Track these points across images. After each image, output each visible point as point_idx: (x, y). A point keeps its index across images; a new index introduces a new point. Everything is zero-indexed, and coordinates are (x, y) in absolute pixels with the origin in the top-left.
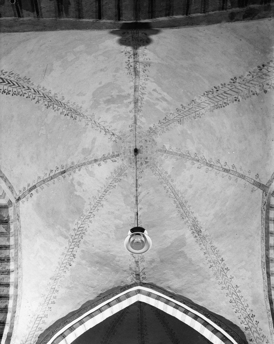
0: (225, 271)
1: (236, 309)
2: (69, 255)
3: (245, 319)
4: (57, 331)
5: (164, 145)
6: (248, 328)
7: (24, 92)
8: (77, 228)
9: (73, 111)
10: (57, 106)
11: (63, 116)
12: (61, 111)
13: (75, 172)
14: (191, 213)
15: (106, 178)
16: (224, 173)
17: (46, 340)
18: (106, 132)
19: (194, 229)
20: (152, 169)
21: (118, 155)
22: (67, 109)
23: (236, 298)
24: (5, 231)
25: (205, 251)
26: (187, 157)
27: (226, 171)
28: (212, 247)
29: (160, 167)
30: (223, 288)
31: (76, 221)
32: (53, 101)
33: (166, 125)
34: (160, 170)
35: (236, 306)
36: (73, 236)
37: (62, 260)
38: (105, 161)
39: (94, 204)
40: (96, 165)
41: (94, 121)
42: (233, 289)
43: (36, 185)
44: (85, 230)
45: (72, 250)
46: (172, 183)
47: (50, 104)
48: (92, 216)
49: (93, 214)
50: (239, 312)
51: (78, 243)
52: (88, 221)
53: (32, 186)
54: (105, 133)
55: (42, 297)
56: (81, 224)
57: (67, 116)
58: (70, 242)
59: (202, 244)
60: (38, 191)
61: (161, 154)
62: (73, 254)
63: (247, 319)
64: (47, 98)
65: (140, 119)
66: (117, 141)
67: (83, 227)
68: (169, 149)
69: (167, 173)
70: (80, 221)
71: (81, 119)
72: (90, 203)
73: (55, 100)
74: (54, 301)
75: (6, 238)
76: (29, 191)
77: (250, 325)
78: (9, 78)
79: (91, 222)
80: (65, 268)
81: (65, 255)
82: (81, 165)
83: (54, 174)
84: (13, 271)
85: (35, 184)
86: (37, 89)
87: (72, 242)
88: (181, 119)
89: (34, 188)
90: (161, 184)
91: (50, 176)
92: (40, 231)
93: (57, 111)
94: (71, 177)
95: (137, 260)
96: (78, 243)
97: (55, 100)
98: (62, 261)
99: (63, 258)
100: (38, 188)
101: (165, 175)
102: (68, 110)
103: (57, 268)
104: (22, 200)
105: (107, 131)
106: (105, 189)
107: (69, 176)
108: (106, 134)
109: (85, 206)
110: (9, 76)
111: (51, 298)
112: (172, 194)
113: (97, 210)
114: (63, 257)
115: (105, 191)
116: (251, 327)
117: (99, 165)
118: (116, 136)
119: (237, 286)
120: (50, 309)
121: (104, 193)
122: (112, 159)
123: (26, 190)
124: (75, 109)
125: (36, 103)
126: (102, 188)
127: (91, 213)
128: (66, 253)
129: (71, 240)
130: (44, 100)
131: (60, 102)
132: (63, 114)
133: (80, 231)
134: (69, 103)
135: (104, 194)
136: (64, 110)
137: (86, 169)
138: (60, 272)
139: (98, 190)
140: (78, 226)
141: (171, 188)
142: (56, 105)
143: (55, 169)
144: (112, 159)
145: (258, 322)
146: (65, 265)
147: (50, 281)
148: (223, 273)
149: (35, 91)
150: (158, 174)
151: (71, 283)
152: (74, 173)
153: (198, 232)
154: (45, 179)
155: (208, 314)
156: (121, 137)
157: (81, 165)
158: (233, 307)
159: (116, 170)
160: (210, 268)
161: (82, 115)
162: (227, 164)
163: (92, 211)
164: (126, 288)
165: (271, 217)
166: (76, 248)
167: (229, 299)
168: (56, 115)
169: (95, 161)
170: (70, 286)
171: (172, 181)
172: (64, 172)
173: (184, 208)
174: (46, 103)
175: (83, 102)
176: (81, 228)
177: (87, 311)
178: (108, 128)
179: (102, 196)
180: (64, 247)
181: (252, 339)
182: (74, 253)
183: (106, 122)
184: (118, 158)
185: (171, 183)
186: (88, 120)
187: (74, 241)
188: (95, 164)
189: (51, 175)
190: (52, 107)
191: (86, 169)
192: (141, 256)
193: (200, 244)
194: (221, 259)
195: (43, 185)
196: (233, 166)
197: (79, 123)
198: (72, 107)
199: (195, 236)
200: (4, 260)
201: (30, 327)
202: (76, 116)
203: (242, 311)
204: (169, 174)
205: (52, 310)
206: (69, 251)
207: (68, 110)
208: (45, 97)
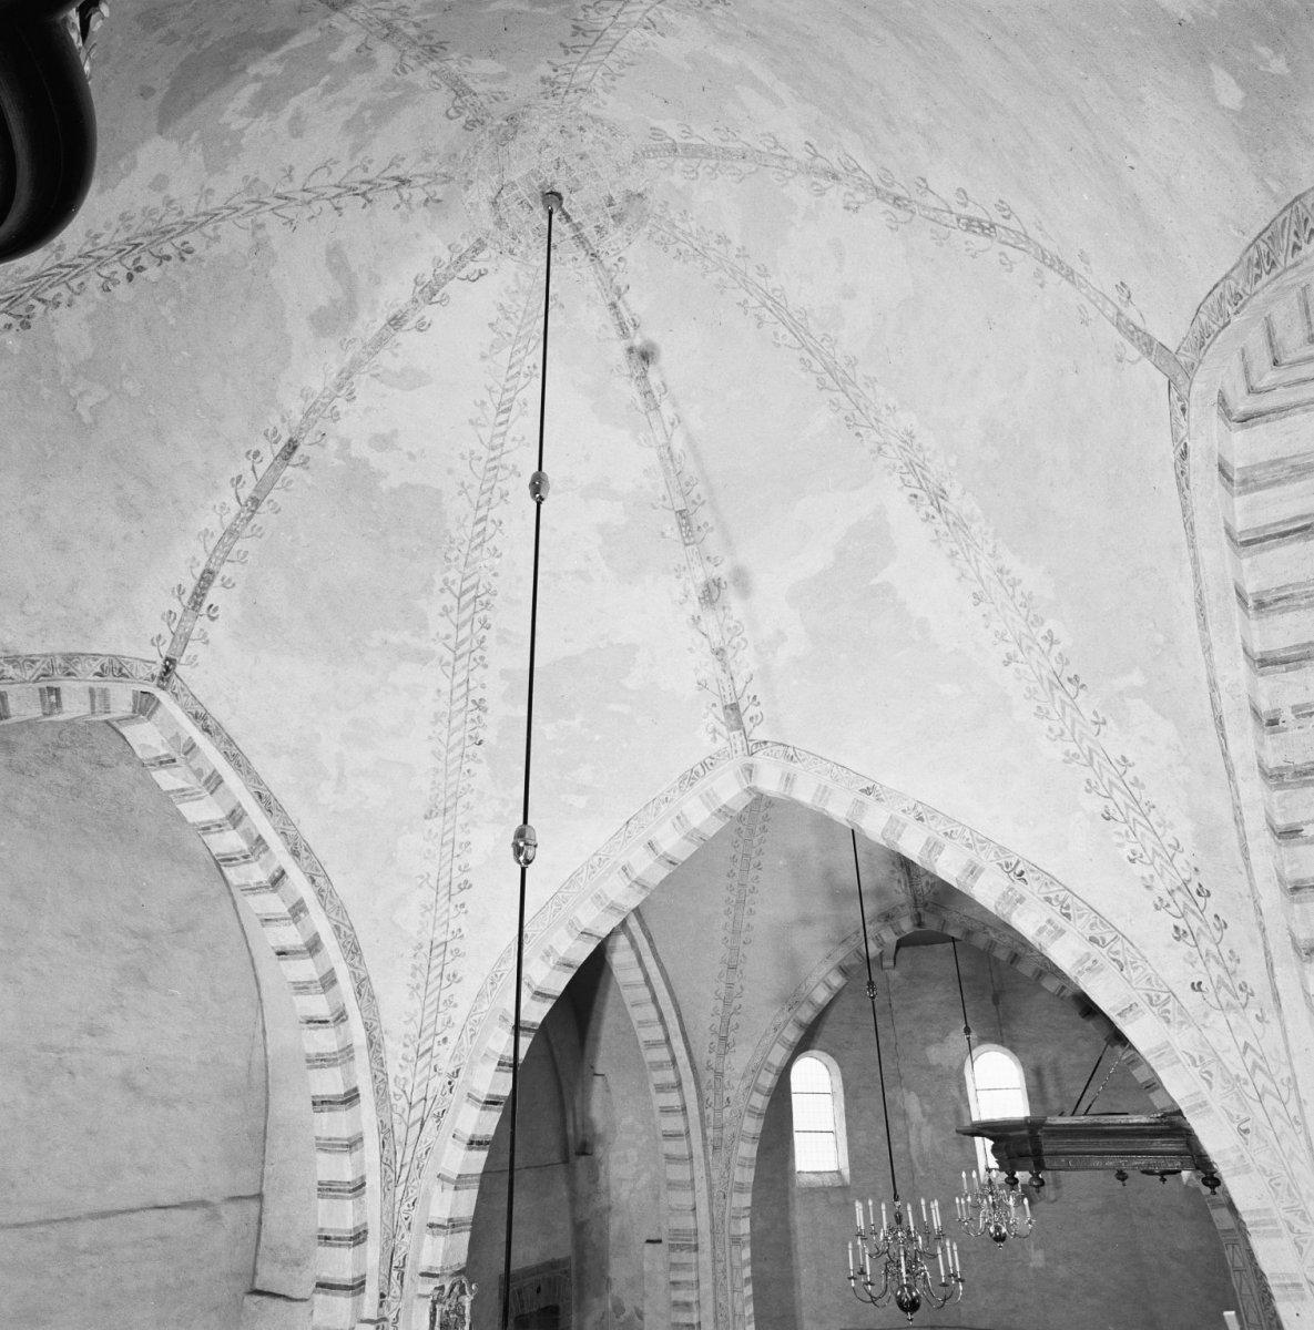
0: (1070, 688)
1: (1134, 846)
2: (461, 710)
3: (1171, 893)
5: (655, 124)
6: (1185, 932)
8: (450, 601)
9: (146, 241)
10: (64, 285)
11: (122, 291)
12: (94, 282)
13: (335, 417)
14: (884, 411)
15: (484, 357)
16: (970, 236)
17: (479, 1011)
18: (364, 194)
19: (914, 482)
20: (657, 237)
21: (479, 246)
22: (115, 258)
23: (1127, 806)
25: (977, 587)
26: (777, 162)
27: (978, 230)
28: (1001, 571)
29: (683, 221)
30: (1070, 758)
33: (604, 50)
34: (690, 234)
35: (1133, 839)
36: (448, 637)
37: (444, 738)
38: (435, 299)
39: (477, 484)
40: (407, 338)
41: (279, 197)
42: (1109, 766)
43: (211, 567)
44: (487, 592)
46: (763, 279)
48: (491, 529)
49: (493, 521)
50: (1145, 859)
51: (478, 653)
52: (486, 554)
53: (194, 583)
54: (362, 201)
55: (420, 886)
56: (463, 581)
57: (143, 274)
58: (448, 664)
59: (960, 556)
61: (662, 165)
62: (474, 701)
63: (1179, 896)
65: (470, 70)
66: (438, 197)
67: (476, 586)
68: (686, 137)
69: (730, 242)
71: (212, 234)
72: (462, 484)
73: (26, 285)
74: (466, 882)
77: (1195, 923)
79: (496, 553)
81: (445, 720)
87: (456, 660)
88: (649, 15)
89: (210, 582)
90: (722, 293)
91: (243, 501)
93: (78, 299)
94: (332, 445)
95: (717, 646)
96: (478, 653)
100: (226, 571)
101: (721, 248)
102: (121, 259)
103: (437, 771)
104: (183, 660)
105: (365, 187)
106: (497, 401)
107: (323, 446)
108: (370, 201)
111: (454, 876)
112: (783, 331)
113: (502, 497)
115: (503, 408)
116: (1198, 935)
117: (422, 327)
118: (421, 181)
119: (1124, 759)
121: (502, 417)
122: (463, 274)
123: (178, 618)
124: (150, 226)
126: (483, 403)
129: (449, 657)
131: (60, 266)
132: (116, 283)
133: (468, 605)
135: (501, 424)
136: (105, 272)
137: (376, 376)
139: (471, 422)
140: (452, 592)
141: (769, 303)
142: (50, 286)
143: (248, 465)
144: (463, 274)
145: (1226, 925)
146: (458, 750)
148: (1058, 694)
150: (691, 251)
152: (335, 421)
153: (936, 495)
155: (1018, 862)
156: (443, 170)
158: (1119, 840)
159: (506, 301)
160: (1006, 664)
161: (202, 219)
162: (971, 195)
163: (481, 513)
164: (697, 773)
165: (998, 956)
166: (479, 671)
167: (1096, 805)
168: (92, 308)
169: (396, 324)
171: (764, 272)
172: (292, 446)
173: (850, 389)
175: (159, 183)
176: (467, 591)
178: (359, 175)
179: (497, 436)
181: (1200, 983)
182: (476, 695)
183: (327, 165)
184: (482, 255)
185: (761, 281)
186: (247, 214)
187: (459, 652)
188: (400, 336)
189: (246, 492)
190: (40, 307)
191: (376, 376)
192: (732, 626)
193: (953, 554)
194: (1043, 632)
195: (237, 547)
196: (1005, 210)
197: (216, 249)
198: (131, 233)
199: (928, 515)
201: (418, 987)
202: (178, 242)
203: (1157, 860)
204: (737, 242)
205: (470, 911)
206: (455, 696)
207: (121, 259)
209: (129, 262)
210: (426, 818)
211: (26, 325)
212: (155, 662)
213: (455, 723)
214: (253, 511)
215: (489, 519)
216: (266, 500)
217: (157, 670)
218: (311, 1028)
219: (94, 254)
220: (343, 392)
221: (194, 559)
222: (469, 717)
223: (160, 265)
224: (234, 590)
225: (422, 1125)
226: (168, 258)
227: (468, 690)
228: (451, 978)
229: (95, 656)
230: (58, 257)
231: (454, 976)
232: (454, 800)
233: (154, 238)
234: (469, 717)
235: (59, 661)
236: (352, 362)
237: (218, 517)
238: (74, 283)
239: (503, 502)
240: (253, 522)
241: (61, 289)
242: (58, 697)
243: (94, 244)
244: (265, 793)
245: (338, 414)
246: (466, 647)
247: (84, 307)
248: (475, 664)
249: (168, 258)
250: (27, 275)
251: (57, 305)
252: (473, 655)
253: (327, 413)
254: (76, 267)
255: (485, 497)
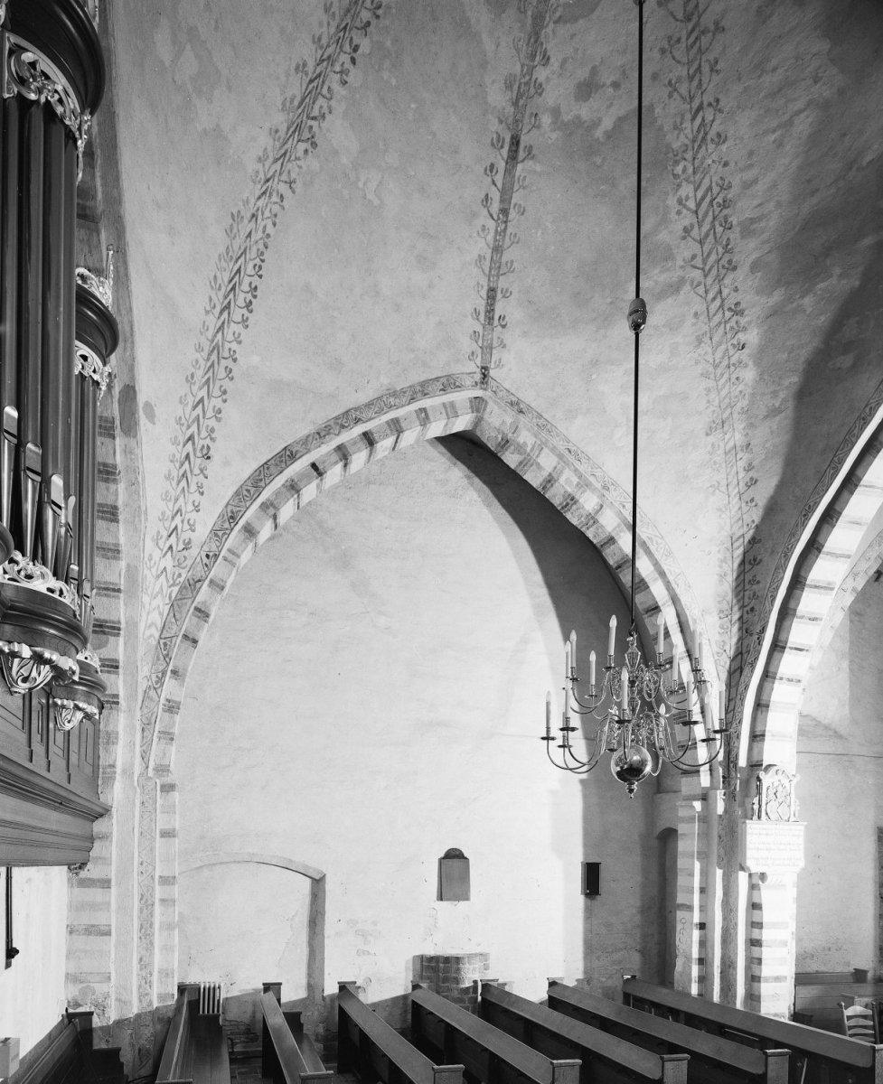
2: (720, 323)
4: (793, 547)
7: (260, 234)
8: (688, 219)
24: (521, 458)
31: (672, 201)
32: (299, 121)
36: (694, 257)
45: (718, 302)
47: (306, 135)
52: (711, 147)
53: (484, 302)
56: (696, 190)
57: (360, 51)
60: (507, 291)
62: (730, 309)
64: (288, 146)
70: (684, 184)
73: (300, 111)
74: (752, 479)
75: (534, 467)
76: (489, 324)
78: (223, 289)
80: (732, 368)
81: (706, 339)
82: (532, 40)
83: (498, 194)
84: (602, 506)
85: (486, 288)
86: (259, 186)
87: (706, 276)
92: (595, 363)
93: (333, 103)
97: (300, 111)
98: (711, 361)
99: (710, 350)
104: (492, 365)
109: (659, 122)
110: (220, 289)
114: (706, 347)
120: (754, 504)
123: (481, 335)
125: (294, 192)
127: (700, 108)
128: (706, 328)
129: (697, 274)
130: (293, 158)
131: (311, 81)
134: (320, 39)
136: (338, 68)
138: (724, 393)
140: (688, 209)
147: (711, 439)
149: (264, 193)
151: (775, 394)
154: (496, 240)
157: (532, 40)
163: (696, 104)
170: (777, 405)
172: (515, 142)
174: (302, 146)
177: (858, 438)
180: (690, 320)
187: (707, 268)
195: (504, 259)
200: (567, 504)
206: (712, 311)
208: (285, 154)
209: (347, 48)
210: (707, 434)
211: (314, 145)
212: (475, 373)
213: (716, 339)
214: (506, 222)
215: (705, 103)
216: (512, 206)
217: (478, 377)
218: (650, 616)
219: (325, 57)
220: (537, 58)
221: (478, 283)
222: (728, 326)
223: (366, 35)
224: (512, 297)
225: (741, 672)
226: (368, 24)
227: (723, 300)
228: (752, 562)
229: (437, 379)
230: (307, 74)
231: (755, 560)
232: (729, 411)
233: (352, 11)
234: (728, 327)
235: (418, 388)
236: (534, 18)
237: (483, 240)
238: (325, 91)
239: (714, 74)
240: (508, 232)
241: (321, 101)
242: (426, 414)
243: (321, 47)
244: (573, 449)
245: (541, 85)
246: (713, 257)
247: (340, 108)
248: (724, 271)
249: (368, 24)
250: (296, 103)
251: (323, 116)
252: (722, 262)
253: (532, 91)
254: (319, 75)
255: (695, 83)
